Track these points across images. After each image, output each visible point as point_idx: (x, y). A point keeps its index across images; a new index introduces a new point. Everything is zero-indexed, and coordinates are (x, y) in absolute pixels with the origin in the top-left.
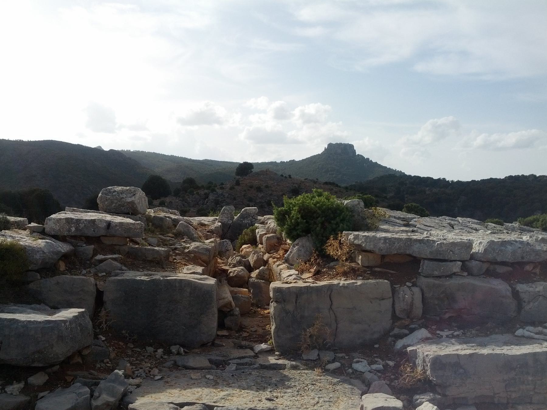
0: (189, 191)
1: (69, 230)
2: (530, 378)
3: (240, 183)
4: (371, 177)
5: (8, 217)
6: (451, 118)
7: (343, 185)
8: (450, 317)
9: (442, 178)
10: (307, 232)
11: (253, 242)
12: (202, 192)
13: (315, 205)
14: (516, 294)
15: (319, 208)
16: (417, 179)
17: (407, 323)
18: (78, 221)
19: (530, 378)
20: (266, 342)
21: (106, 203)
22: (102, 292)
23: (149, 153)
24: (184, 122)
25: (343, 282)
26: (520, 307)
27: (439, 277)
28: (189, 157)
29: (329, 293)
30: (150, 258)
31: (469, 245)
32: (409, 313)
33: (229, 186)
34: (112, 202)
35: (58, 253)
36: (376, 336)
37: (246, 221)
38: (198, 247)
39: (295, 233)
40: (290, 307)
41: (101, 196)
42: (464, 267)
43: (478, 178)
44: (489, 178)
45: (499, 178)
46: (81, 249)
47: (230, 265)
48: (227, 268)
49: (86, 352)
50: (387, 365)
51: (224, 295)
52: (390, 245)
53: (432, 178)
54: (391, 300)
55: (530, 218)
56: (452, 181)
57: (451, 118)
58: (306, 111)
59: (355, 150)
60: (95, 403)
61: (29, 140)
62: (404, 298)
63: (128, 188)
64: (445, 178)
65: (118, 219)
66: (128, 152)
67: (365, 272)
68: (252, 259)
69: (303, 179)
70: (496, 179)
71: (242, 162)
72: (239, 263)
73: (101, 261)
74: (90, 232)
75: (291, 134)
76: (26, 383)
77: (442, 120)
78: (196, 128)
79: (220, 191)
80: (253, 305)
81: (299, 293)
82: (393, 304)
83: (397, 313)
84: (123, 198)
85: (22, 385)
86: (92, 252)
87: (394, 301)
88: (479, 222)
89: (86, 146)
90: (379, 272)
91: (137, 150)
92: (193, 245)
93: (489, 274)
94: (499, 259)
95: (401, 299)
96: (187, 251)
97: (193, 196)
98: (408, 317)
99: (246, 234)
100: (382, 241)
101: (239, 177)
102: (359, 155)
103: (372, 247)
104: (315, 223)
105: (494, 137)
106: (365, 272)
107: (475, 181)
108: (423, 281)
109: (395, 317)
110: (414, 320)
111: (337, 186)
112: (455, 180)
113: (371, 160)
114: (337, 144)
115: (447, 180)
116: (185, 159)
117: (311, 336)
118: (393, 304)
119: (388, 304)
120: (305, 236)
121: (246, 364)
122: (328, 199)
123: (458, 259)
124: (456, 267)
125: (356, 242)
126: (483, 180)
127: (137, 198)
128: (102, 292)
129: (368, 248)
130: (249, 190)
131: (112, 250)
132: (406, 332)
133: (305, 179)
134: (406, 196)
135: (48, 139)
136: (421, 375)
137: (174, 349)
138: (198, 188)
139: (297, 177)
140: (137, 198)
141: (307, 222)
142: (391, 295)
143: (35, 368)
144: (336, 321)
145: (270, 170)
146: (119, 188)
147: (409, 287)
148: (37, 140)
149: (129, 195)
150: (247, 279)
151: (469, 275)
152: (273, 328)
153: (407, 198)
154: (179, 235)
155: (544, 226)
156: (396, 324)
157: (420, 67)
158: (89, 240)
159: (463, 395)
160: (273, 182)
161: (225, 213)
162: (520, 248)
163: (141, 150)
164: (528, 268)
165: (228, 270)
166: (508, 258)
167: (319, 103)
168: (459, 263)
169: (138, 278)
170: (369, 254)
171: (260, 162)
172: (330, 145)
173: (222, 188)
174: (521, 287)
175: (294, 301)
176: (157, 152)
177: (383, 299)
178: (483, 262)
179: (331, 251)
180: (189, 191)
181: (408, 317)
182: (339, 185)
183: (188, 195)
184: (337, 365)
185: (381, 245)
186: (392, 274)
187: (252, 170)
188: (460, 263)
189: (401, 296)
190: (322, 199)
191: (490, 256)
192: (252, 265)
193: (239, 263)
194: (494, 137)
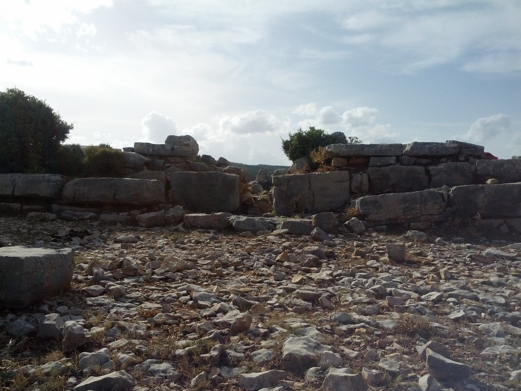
1: (149, 151)
6: (500, 116)
14: (427, 172)
20: (270, 211)
24: (237, 130)
26: (430, 180)
27: (380, 167)
28: (244, 163)
35: (142, 160)
40: (284, 188)
42: (398, 159)
52: (349, 149)
54: (348, 183)
57: (500, 116)
58: (354, 115)
73: (168, 167)
76: (129, 213)
77: (490, 119)
78: (249, 135)
83: (353, 189)
84: (182, 141)
85: (128, 213)
86: (162, 163)
94: (420, 153)
100: (345, 147)
110: (364, 194)
119: (346, 184)
123: (393, 155)
124: (393, 160)
125: (329, 150)
142: (348, 178)
144: (313, 196)
149: (185, 140)
157: (469, 67)
158: (161, 157)
159: (379, 219)
161: (261, 174)
162: (435, 146)
167: (366, 107)
168: (394, 157)
174: (431, 168)
177: (344, 182)
185: (344, 149)
189: (355, 179)
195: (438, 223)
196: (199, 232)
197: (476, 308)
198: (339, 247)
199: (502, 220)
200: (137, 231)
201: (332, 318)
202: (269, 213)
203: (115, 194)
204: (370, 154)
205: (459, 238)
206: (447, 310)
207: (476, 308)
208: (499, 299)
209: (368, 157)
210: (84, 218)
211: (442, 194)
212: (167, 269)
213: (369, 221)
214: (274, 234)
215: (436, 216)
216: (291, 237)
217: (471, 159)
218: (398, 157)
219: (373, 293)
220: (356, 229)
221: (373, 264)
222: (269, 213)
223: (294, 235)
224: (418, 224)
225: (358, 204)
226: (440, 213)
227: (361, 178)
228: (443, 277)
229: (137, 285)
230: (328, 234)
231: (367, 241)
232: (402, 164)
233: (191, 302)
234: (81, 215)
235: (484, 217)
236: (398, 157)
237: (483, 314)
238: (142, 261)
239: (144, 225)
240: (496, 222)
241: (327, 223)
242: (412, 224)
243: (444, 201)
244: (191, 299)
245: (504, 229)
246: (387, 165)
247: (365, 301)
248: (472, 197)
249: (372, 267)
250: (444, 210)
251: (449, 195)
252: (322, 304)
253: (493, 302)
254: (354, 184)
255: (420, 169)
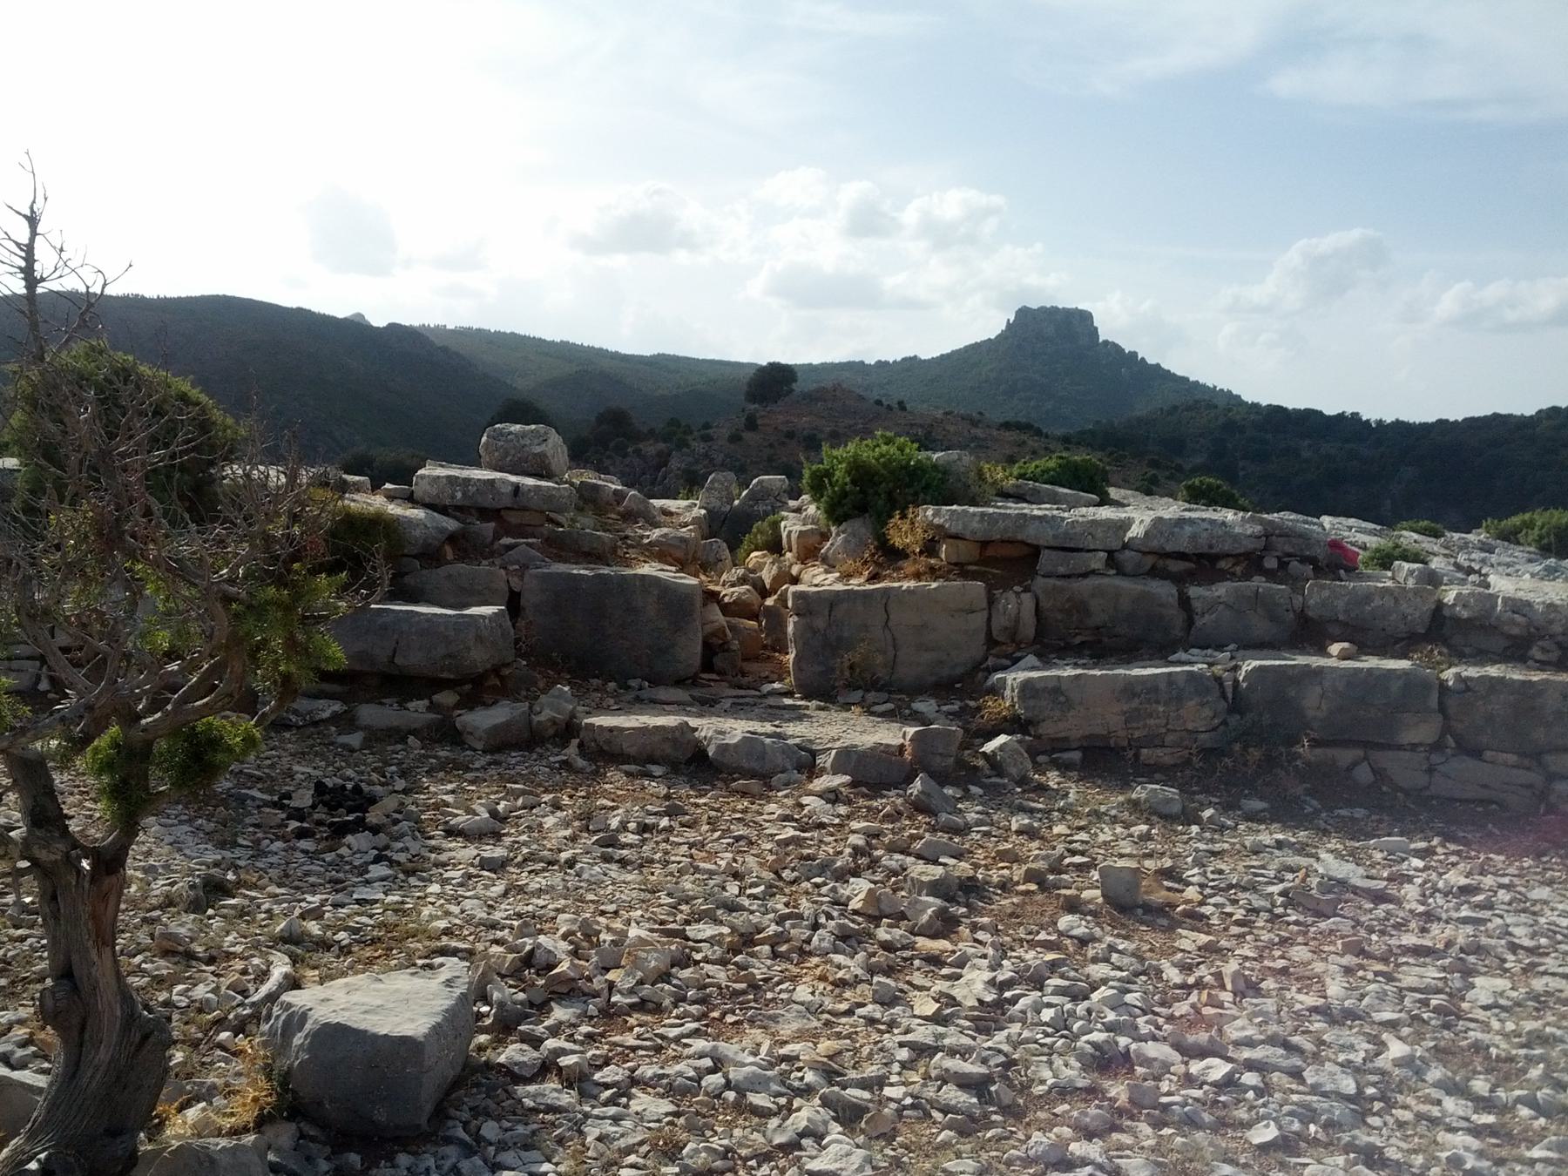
0: (612, 445)
1: (453, 497)
2: (1161, 709)
3: (759, 422)
4: (1141, 409)
5: (345, 476)
6: (1356, 234)
7: (1059, 432)
8: (1083, 643)
9: (1349, 411)
10: (861, 509)
11: (775, 547)
12: (651, 448)
13: (877, 460)
14: (1185, 602)
15: (884, 465)
16: (1277, 416)
17: (1010, 650)
18: (467, 481)
19: (1161, 709)
20: (781, 680)
21: (496, 454)
22: (519, 595)
23: (497, 333)
25: (906, 585)
26: (1190, 622)
28: (612, 348)
29: (884, 601)
30: (586, 549)
31: (1126, 525)
32: (1013, 633)
33: (725, 432)
34: (507, 454)
35: (442, 530)
36: (959, 671)
37: (761, 508)
38: (665, 535)
39: (840, 511)
40: (820, 623)
41: (487, 443)
42: (1112, 558)
43: (1456, 414)
44: (1489, 413)
45: (1519, 414)
46: (472, 528)
47: (724, 585)
48: (717, 588)
49: (506, 672)
50: (967, 705)
51: (712, 618)
53: (1320, 413)
54: (985, 613)
55: (1516, 520)
56: (1380, 423)
59: (1096, 329)
60: (536, 719)
61: (162, 296)
62: (1005, 608)
63: (533, 427)
64: (1357, 414)
65: (530, 481)
66: (440, 331)
67: (950, 572)
68: (767, 575)
69: (939, 414)
70: (1510, 416)
71: (763, 362)
72: (742, 580)
73: (509, 548)
74: (488, 501)
75: (892, 282)
76: (431, 702)
78: (620, 260)
79: (699, 447)
80: (765, 647)
81: (833, 601)
82: (989, 619)
83: (995, 633)
85: (426, 702)
87: (990, 614)
88: (1378, 527)
89: (322, 312)
90: (974, 572)
91: (466, 325)
92: (656, 534)
93: (1154, 573)
94: (1169, 548)
95: (1001, 610)
96: (646, 541)
97: (627, 461)
98: (1013, 641)
99: (759, 531)
100: (977, 518)
101: (756, 406)
102: (1106, 342)
103: (960, 527)
104: (876, 493)
105: (1493, 292)
106: (950, 572)
107: (1447, 421)
108: (1040, 583)
109: (991, 642)
111: (1039, 433)
112: (1389, 419)
113: (1143, 359)
114: (1043, 310)
115: (1364, 419)
116: (601, 353)
117: (851, 667)
118: (989, 619)
119: (979, 620)
120: (859, 516)
121: (747, 704)
122: (901, 449)
124: (1097, 561)
125: (937, 521)
126: (1472, 419)
127: (550, 446)
128: (519, 595)
129: (953, 531)
130: (784, 443)
131: (519, 531)
132: (1008, 662)
133: (946, 414)
134: (1241, 464)
135: (215, 293)
136: (1008, 709)
137: (633, 683)
138: (638, 437)
139: (925, 406)
140: (550, 446)
141: (861, 491)
142: (985, 605)
143: (442, 680)
145: (844, 386)
146: (517, 428)
147: (1017, 594)
148: (183, 295)
149: (536, 441)
150: (756, 607)
151: (1117, 574)
152: (791, 657)
153: (1243, 469)
154: (630, 516)
155: (1545, 541)
156: (993, 652)
157: (1287, 83)
158: (486, 513)
159: (1061, 735)
160: (852, 422)
163: (476, 325)
164: (1223, 564)
165: (719, 593)
166: (1183, 545)
169: (575, 572)
170: (960, 543)
171: (816, 361)
172: (1023, 313)
173: (707, 439)
174: (1194, 591)
175: (827, 613)
176: (522, 333)
178: (1144, 553)
179: (898, 541)
180: (612, 445)
181: (1013, 641)
182: (1045, 431)
183: (609, 457)
184: (890, 706)
185: (975, 525)
186: (994, 575)
187: (794, 386)
188: (1103, 555)
189: (1000, 606)
190: (893, 450)
191: (1155, 544)
192: (768, 587)
193: (742, 580)
194: (1493, 292)
195: (1208, 753)
196: (628, 774)
197: (1300, 1110)
198: (979, 837)
199: (1359, 753)
200: (468, 769)
201: (1030, 1153)
202: (776, 685)
203: (395, 652)
204: (1042, 542)
205: (1257, 805)
206: (1242, 1114)
207: (1300, 1110)
208: (1345, 1082)
209: (1035, 551)
210: (318, 718)
211: (1218, 680)
212: (639, 974)
213: (1038, 737)
214: (818, 789)
215: (1202, 736)
216: (856, 795)
217: (1294, 565)
218: (1111, 553)
219: (1092, 1055)
220: (1013, 771)
221: (1072, 928)
222: (776, 685)
223: (864, 789)
224: (1159, 752)
225: (1013, 691)
226: (1214, 729)
227: (1016, 605)
228: (1229, 987)
229: (595, 1034)
230: (943, 787)
231: (1039, 810)
232: (1121, 572)
233: (731, 1095)
234: (310, 712)
235: (1315, 743)
236: (1111, 553)
237: (1312, 1128)
238: (571, 943)
239: (479, 746)
240: (1345, 756)
241: (941, 754)
242: (1144, 751)
243: (1223, 695)
244: (728, 1085)
245: (1364, 774)
246: (1085, 575)
247: (1081, 1083)
248: (1293, 694)
249: (1071, 937)
250: (1224, 723)
251: (1236, 681)
252: (999, 1099)
253: (1332, 1092)
254: (1000, 622)
255: (1164, 590)
